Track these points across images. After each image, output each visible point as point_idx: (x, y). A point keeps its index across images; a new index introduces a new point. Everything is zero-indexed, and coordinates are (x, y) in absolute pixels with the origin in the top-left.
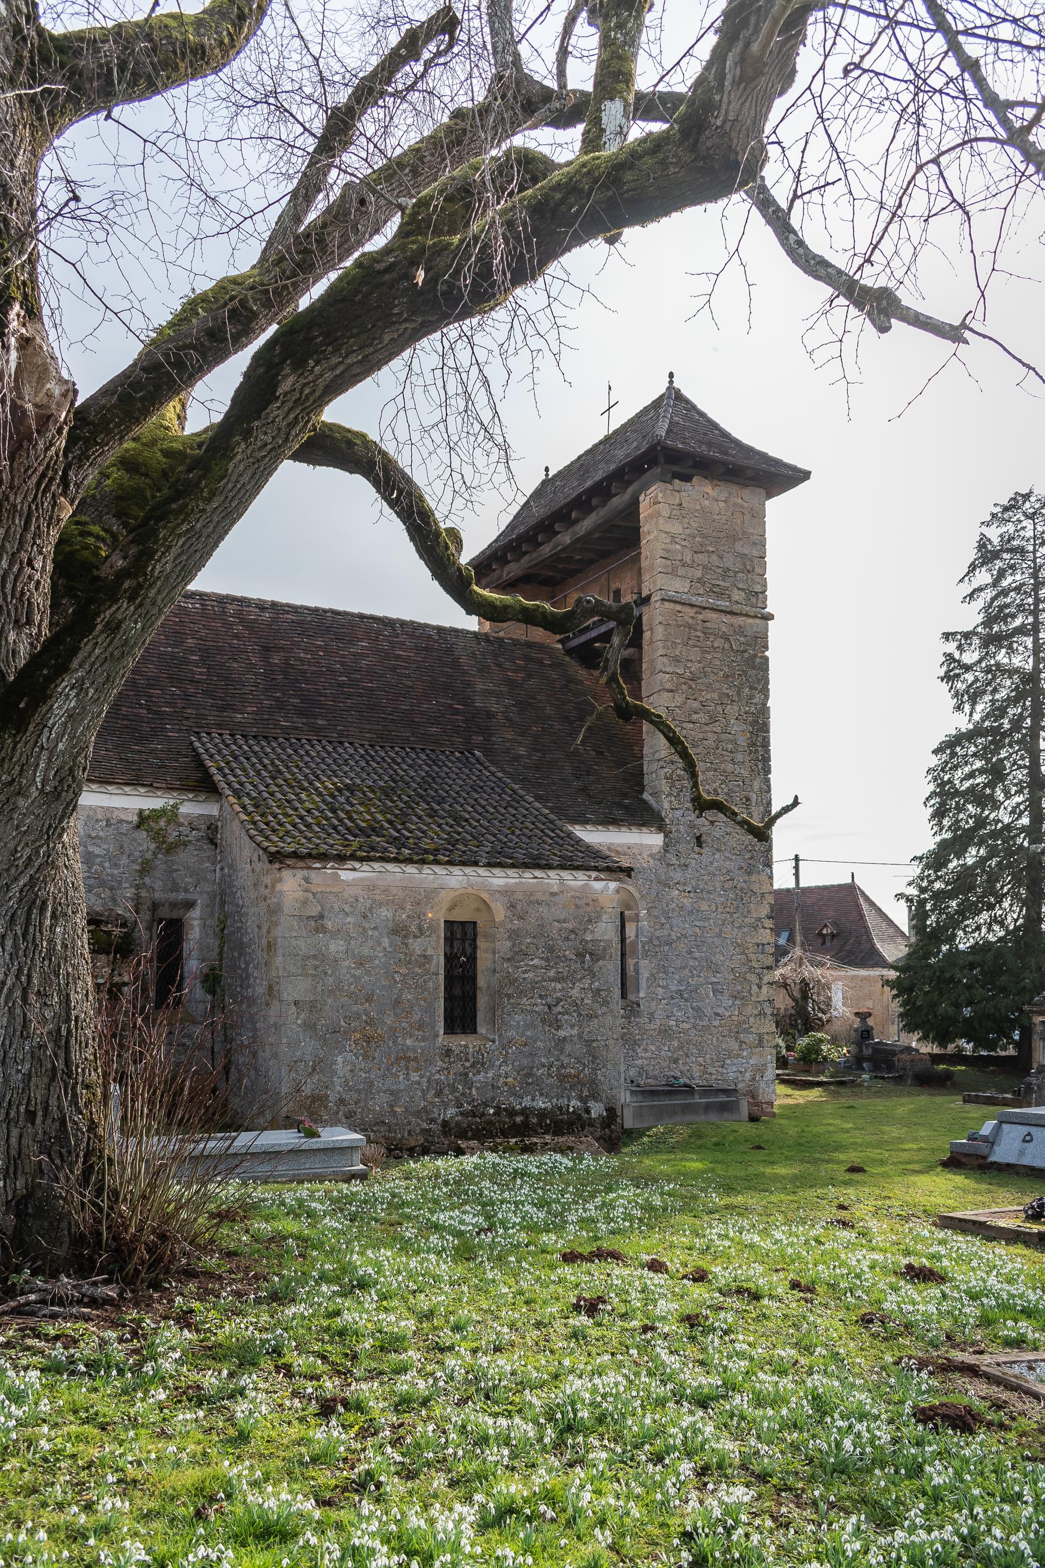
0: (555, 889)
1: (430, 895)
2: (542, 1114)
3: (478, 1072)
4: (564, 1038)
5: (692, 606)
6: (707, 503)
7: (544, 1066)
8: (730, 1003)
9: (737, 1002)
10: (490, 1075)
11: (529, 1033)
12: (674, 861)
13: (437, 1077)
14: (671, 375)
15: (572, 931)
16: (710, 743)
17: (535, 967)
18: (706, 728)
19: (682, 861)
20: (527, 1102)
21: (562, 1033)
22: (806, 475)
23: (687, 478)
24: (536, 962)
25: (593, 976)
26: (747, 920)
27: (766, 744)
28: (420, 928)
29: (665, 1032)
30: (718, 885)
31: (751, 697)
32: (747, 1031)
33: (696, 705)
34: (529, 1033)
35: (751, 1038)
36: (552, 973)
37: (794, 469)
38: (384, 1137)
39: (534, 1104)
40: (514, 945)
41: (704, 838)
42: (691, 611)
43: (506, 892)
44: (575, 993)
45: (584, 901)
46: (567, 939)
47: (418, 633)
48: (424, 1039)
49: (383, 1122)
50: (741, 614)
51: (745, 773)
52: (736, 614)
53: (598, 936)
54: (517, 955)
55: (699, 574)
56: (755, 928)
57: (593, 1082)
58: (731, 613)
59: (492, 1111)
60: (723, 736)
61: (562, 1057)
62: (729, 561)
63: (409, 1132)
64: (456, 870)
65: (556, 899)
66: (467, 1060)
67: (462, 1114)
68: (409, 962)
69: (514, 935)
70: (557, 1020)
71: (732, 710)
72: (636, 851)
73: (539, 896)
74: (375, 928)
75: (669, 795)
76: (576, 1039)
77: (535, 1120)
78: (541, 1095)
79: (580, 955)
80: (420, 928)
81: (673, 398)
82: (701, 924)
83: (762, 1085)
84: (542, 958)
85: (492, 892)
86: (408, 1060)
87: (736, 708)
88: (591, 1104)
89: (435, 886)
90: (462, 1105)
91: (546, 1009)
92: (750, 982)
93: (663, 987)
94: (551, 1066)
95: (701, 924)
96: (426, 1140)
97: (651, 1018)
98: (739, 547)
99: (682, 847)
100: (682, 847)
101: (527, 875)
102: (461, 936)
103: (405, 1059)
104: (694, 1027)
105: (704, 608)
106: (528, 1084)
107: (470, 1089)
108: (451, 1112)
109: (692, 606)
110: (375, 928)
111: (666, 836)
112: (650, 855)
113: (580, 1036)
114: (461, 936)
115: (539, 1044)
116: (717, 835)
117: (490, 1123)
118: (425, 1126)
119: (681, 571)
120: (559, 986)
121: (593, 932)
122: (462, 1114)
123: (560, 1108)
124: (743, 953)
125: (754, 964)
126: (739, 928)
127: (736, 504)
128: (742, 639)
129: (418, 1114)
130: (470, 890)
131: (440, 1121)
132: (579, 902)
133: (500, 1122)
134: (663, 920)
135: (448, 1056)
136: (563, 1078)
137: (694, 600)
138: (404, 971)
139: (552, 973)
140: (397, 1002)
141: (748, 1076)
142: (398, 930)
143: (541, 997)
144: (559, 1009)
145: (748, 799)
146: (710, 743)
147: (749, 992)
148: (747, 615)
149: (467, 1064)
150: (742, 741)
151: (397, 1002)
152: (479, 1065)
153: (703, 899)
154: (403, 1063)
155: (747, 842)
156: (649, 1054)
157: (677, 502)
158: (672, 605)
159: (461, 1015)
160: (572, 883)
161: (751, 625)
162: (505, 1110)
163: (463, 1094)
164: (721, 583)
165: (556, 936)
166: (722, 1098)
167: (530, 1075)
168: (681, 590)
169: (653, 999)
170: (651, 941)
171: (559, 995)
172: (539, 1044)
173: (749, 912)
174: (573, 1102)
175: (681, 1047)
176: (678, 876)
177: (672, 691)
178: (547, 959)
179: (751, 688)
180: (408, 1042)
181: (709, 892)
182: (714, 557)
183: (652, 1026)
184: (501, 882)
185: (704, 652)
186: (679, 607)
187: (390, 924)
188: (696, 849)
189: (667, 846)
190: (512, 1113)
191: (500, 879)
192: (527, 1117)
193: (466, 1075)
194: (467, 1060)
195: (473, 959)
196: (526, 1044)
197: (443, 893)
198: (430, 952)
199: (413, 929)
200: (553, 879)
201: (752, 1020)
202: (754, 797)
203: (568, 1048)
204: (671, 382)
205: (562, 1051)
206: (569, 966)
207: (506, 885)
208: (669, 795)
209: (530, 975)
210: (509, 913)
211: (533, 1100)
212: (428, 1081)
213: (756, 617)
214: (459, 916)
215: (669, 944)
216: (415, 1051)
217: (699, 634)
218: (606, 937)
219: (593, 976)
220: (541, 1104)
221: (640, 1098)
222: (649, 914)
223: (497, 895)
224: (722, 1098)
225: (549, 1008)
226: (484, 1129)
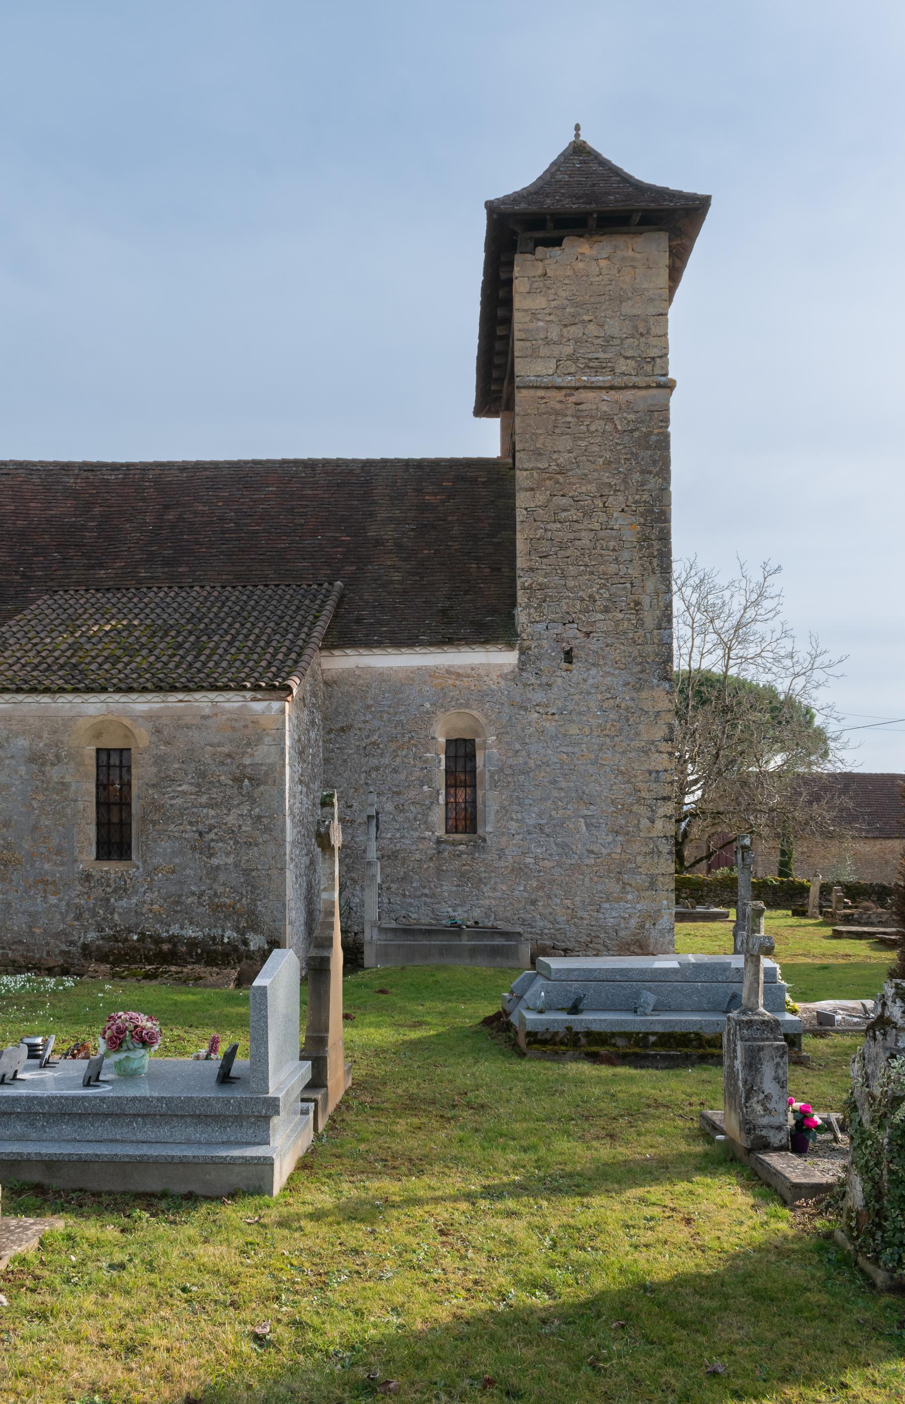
0: (207, 711)
1: (68, 722)
2: (193, 943)
3: (121, 898)
4: (218, 867)
5: (559, 388)
6: (581, 265)
7: (193, 894)
8: (610, 838)
9: (619, 838)
10: (134, 901)
11: (177, 861)
12: (533, 680)
13: (77, 901)
14: (577, 128)
15: (229, 755)
16: (586, 542)
18: (577, 526)
19: (544, 680)
20: (175, 930)
21: (215, 861)
23: (557, 242)
24: (185, 787)
25: (253, 801)
26: (636, 744)
27: (665, 538)
28: (58, 757)
29: (520, 871)
30: (592, 704)
32: (634, 872)
33: (564, 501)
34: (177, 861)
35: (640, 880)
36: (204, 799)
37: (694, 197)
38: (22, 955)
39: (183, 932)
40: (159, 771)
41: (575, 652)
43: (150, 717)
45: (243, 723)
46: (222, 763)
47: (339, 470)
48: (62, 864)
49: (21, 942)
50: (626, 387)
51: (634, 571)
52: (621, 388)
53: (258, 760)
54: (164, 781)
55: (569, 349)
56: (646, 752)
57: (252, 913)
58: (612, 388)
59: (135, 937)
60: (603, 534)
61: (215, 886)
62: (614, 327)
63: (48, 952)
64: (92, 698)
65: (209, 722)
66: (108, 886)
67: (103, 938)
68: (46, 789)
69: (160, 760)
70: (209, 848)
71: (616, 501)
72: (482, 672)
73: (188, 720)
74: (12, 757)
75: (528, 606)
77: (184, 949)
78: (191, 923)
79: (238, 780)
80: (58, 757)
81: (579, 153)
82: (570, 749)
83: (654, 933)
84: (192, 784)
85: (135, 718)
86: (46, 883)
87: (621, 498)
88: (250, 936)
89: (72, 714)
90: (103, 930)
92: (638, 816)
93: (517, 821)
94: (202, 894)
95: (570, 749)
96: (66, 961)
97: (501, 853)
98: (627, 308)
99: (543, 665)
100: (543, 665)
101: (170, 699)
102: (113, 765)
103: (44, 883)
104: (559, 865)
105: (577, 388)
107: (112, 914)
108: (92, 935)
109: (559, 388)
110: (12, 757)
111: (522, 653)
112: (500, 676)
113: (236, 865)
114: (113, 765)
116: (594, 648)
117: (134, 948)
118: (64, 947)
119: (544, 351)
120: (212, 813)
121: (252, 755)
122: (103, 938)
123: (214, 939)
124: (628, 782)
126: (624, 752)
127: (624, 259)
128: (632, 417)
129: (57, 935)
130: (110, 717)
131: (79, 944)
132: (236, 725)
133: (145, 949)
134: (518, 747)
135: (89, 881)
136: (217, 908)
137: (559, 381)
138: (41, 797)
139: (204, 799)
140: (35, 828)
141: (633, 922)
142: (36, 759)
143: (191, 823)
144: (212, 836)
145: (637, 603)
146: (586, 542)
147: (637, 826)
148: (634, 387)
149: (109, 890)
150: (630, 536)
151: (35, 828)
152: (122, 890)
154: (40, 887)
156: (498, 894)
157: (540, 271)
159: (114, 841)
160: (227, 705)
162: (150, 936)
163: (104, 919)
164: (601, 355)
166: (499, 942)
167: (177, 903)
168: (544, 372)
169: (503, 834)
171: (212, 821)
173: (637, 734)
174: (228, 933)
175: (541, 887)
176: (538, 696)
177: (532, 489)
178: (198, 785)
179: (643, 472)
180: (47, 866)
182: (592, 327)
183: (502, 864)
184: (145, 707)
185: (575, 439)
186: (541, 393)
187: (27, 754)
188: (564, 665)
189: (522, 666)
190: (158, 940)
191: (143, 704)
192: (175, 945)
193: (108, 900)
194: (108, 886)
195: (127, 785)
196: (173, 872)
197: (81, 721)
198: (68, 779)
199: (51, 757)
200: (203, 701)
201: (640, 859)
202: (646, 600)
203: (222, 877)
204: (577, 135)
205: (215, 880)
206: (224, 792)
207: (151, 710)
209: (178, 801)
210: (155, 739)
211: (182, 928)
212: (68, 905)
213: (649, 387)
214: (113, 742)
215: (527, 773)
216: (53, 875)
217: (569, 419)
219: (253, 801)
220: (190, 932)
221: (390, 936)
223: (141, 721)
224: (499, 942)
225: (201, 834)
226: (127, 954)
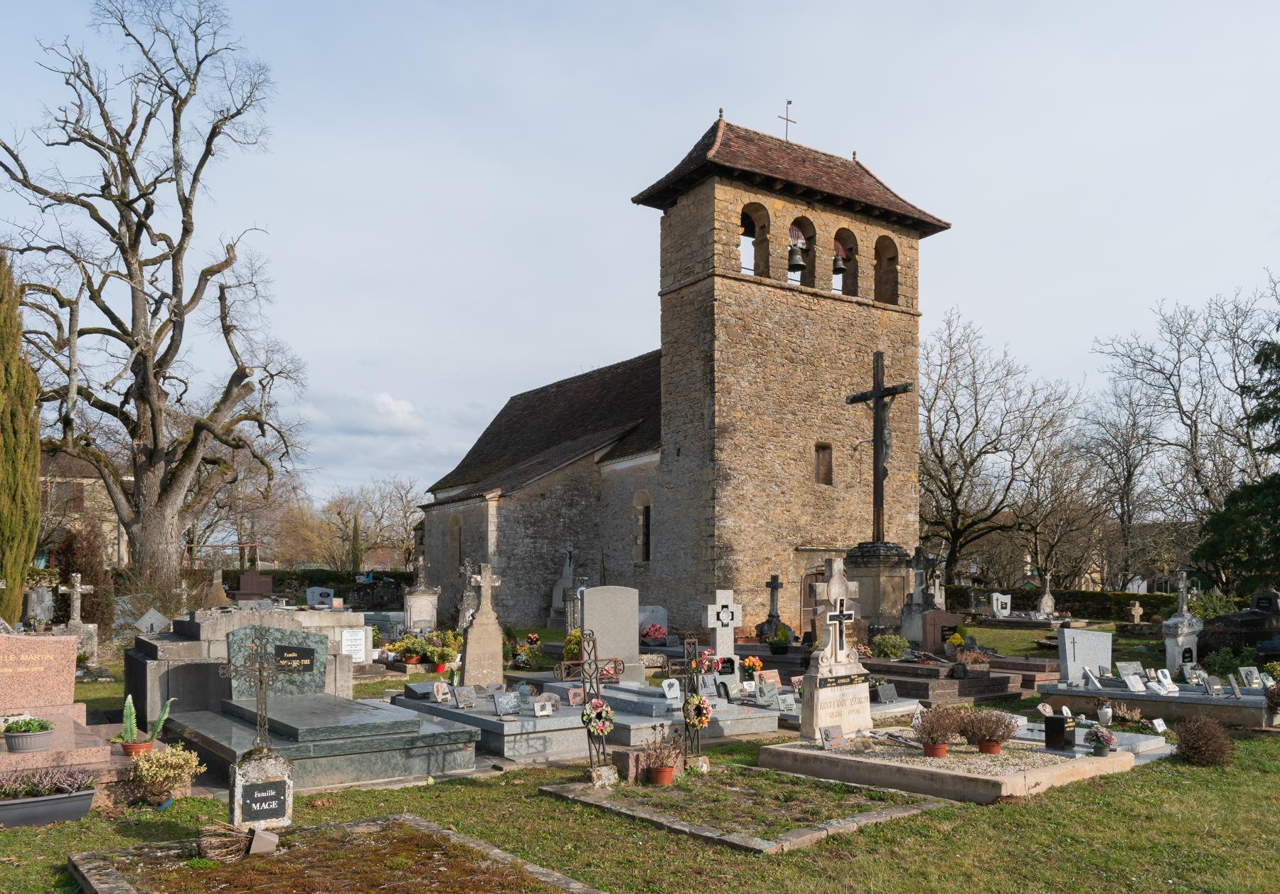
14: (721, 111)
42: (674, 295)
176: (667, 478)
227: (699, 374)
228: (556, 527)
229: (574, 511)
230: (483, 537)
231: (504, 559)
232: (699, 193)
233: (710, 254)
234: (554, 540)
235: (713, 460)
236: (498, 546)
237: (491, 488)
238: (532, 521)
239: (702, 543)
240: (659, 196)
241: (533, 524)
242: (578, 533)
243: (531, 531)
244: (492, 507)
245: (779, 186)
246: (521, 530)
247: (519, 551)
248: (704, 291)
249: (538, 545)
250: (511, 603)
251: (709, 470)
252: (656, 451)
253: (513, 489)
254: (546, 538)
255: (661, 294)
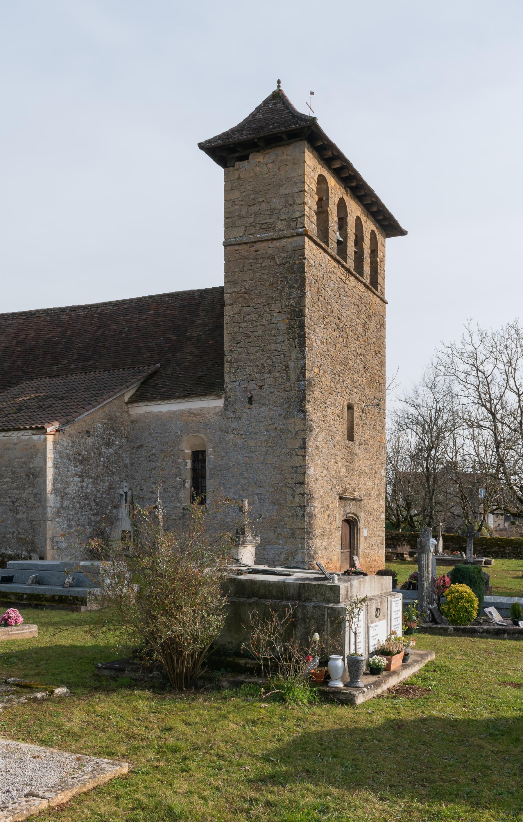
0: (15, 441)
4: (20, 519)
7: (10, 533)
9: (276, 507)
12: (231, 415)
14: (279, 82)
15: (24, 463)
17: (7, 482)
18: (255, 323)
19: (237, 415)
21: (19, 516)
22: (202, 146)
23: (245, 158)
24: (7, 480)
26: (285, 451)
31: (290, 294)
33: (248, 310)
34: (4, 516)
36: (14, 485)
39: (7, 552)
42: (246, 247)
44: (25, 495)
46: (22, 467)
56: (291, 456)
61: (19, 529)
70: (17, 510)
71: (276, 306)
76: (25, 520)
79: (28, 475)
82: (250, 455)
87: (279, 305)
91: (11, 503)
95: (250, 455)
105: (255, 242)
106: (4, 542)
109: (246, 243)
113: (27, 519)
115: (8, 521)
116: (263, 394)
119: (238, 223)
120: (18, 492)
121: (33, 463)
125: (289, 481)
134: (223, 454)
139: (14, 485)
143: (9, 497)
144: (17, 504)
145: (287, 367)
146: (260, 333)
148: (285, 237)
153: (251, 438)
155: (285, 397)
158: (232, 247)
161: (291, 243)
164: (268, 221)
165: (17, 466)
168: (238, 235)
170: (215, 468)
171: (18, 496)
172: (8, 521)
174: (24, 553)
176: (234, 424)
177: (232, 304)
178: (12, 478)
181: (255, 434)
182: (264, 204)
185: (255, 272)
186: (237, 247)
189: (226, 407)
201: (286, 519)
203: (21, 524)
205: (18, 526)
208: (230, 372)
211: (6, 550)
213: (292, 236)
217: (251, 261)
218: (40, 465)
222: (214, 451)
225: (13, 503)
227: (283, 327)
228: (98, 466)
229: (111, 450)
230: (41, 473)
231: (59, 498)
232: (285, 154)
233: (298, 214)
234: (96, 480)
235: (303, 411)
236: (54, 484)
237: (50, 421)
238: (81, 459)
239: (288, 490)
240: (225, 150)
241: (81, 462)
242: (113, 473)
243: (79, 470)
244: (50, 439)
245: (337, 165)
246: (72, 467)
247: (71, 490)
248: (290, 248)
249: (84, 484)
250: (64, 545)
251: (298, 420)
252: (219, 397)
253: (68, 422)
254: (90, 477)
255: (226, 245)
